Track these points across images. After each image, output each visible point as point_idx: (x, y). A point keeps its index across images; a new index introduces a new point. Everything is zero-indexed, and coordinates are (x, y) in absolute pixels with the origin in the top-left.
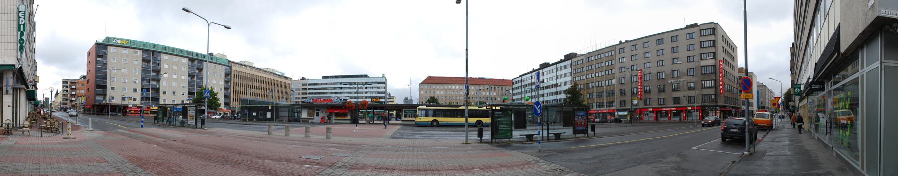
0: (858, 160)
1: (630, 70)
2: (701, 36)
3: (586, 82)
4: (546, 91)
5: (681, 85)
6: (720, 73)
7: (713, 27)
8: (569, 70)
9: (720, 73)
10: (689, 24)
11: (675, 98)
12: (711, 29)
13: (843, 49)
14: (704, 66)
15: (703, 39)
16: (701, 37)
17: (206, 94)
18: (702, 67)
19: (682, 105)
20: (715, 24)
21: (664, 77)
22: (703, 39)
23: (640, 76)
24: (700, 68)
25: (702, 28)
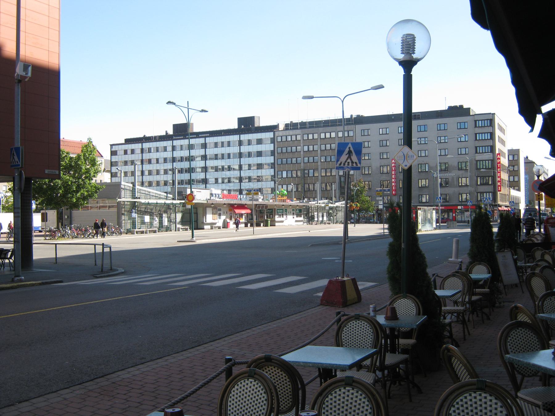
0: (519, 190)
1: (185, 111)
2: (476, 126)
3: (302, 168)
4: (162, 178)
5: (450, 180)
6: (498, 168)
7: (490, 118)
8: (268, 147)
9: (498, 168)
10: (453, 105)
11: (218, 180)
12: (487, 120)
13: (283, 357)
14: (480, 161)
15: (478, 130)
16: (476, 128)
17: (438, 200)
18: (477, 161)
19: (451, 204)
20: (492, 114)
21: (427, 170)
22: (478, 130)
23: (394, 166)
24: (475, 162)
25: (476, 118)
